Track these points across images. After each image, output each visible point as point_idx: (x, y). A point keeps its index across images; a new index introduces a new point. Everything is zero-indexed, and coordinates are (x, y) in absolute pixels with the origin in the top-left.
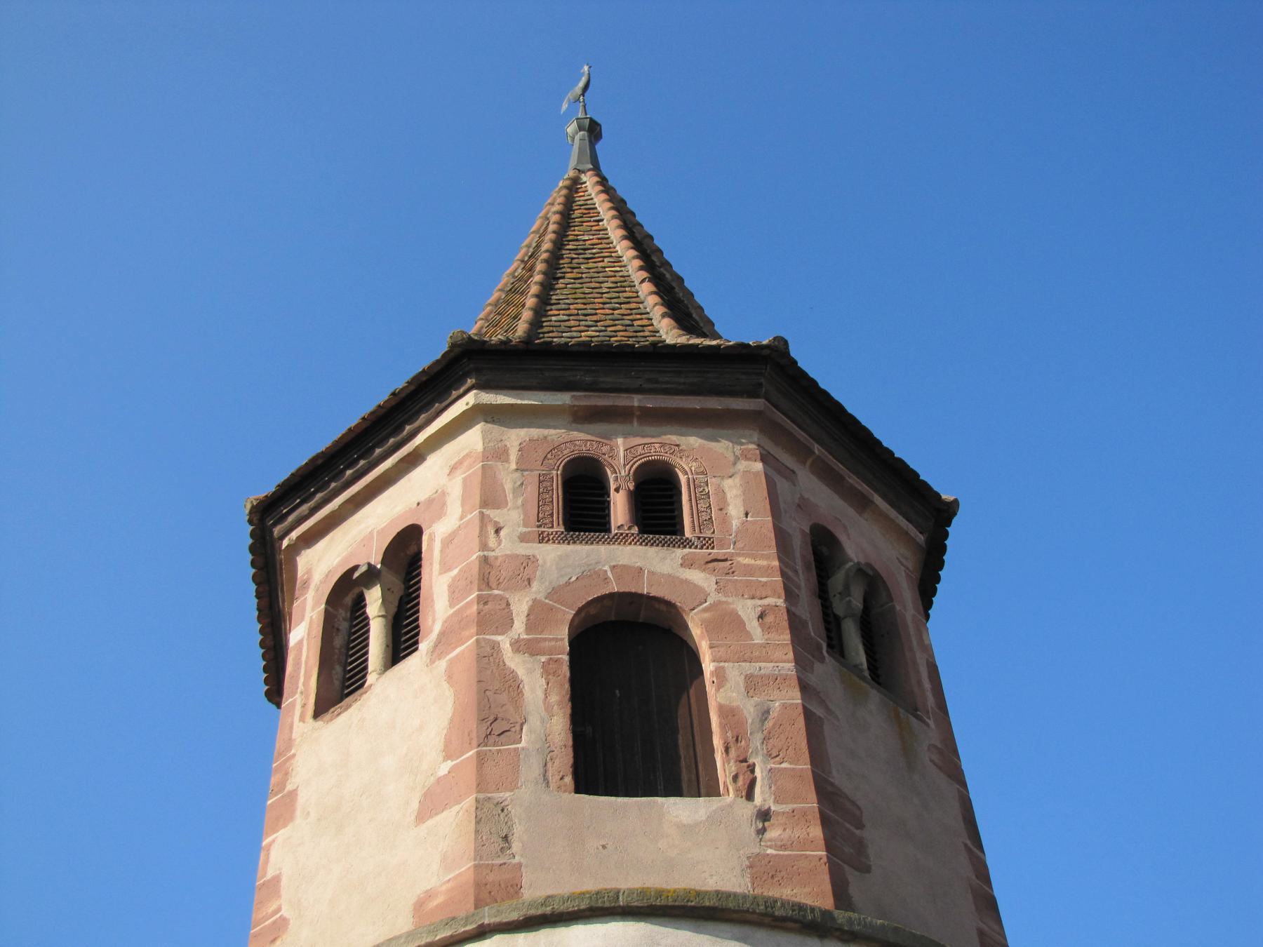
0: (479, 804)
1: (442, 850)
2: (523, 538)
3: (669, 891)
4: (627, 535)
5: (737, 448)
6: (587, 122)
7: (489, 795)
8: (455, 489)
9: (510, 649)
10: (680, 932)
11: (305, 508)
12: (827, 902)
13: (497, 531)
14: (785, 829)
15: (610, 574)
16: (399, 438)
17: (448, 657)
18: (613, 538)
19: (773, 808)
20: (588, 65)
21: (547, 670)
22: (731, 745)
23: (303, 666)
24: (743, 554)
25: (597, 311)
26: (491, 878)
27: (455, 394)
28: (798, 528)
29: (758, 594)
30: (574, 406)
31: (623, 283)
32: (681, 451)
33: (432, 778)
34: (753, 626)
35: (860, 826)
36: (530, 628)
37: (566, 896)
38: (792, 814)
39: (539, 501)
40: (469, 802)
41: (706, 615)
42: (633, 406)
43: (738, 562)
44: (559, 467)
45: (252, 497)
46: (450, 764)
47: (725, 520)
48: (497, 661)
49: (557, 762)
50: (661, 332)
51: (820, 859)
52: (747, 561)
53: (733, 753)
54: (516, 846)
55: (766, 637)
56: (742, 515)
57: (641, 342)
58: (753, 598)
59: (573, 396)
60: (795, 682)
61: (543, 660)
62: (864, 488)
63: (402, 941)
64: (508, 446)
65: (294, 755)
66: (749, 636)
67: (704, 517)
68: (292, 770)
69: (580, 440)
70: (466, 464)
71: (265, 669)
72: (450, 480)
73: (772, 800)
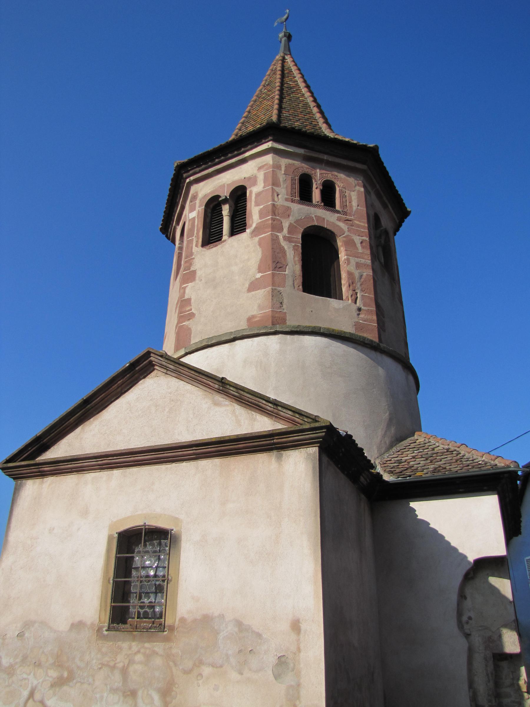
0: (273, 290)
1: (258, 303)
2: (287, 200)
3: (336, 330)
4: (320, 205)
5: (356, 181)
6: (288, 34)
7: (276, 288)
8: (261, 176)
9: (282, 239)
10: (337, 343)
11: (197, 169)
12: (376, 340)
13: (278, 195)
14: (365, 315)
15: (314, 218)
16: (239, 152)
17: (259, 237)
18: (315, 206)
19: (362, 308)
20: (288, 10)
21: (295, 248)
22: (351, 285)
23: (196, 227)
24: (357, 220)
25: (299, 115)
26: (277, 315)
27: (263, 141)
28: (372, 213)
29: (361, 235)
30: (305, 155)
31: (306, 105)
32: (338, 178)
33: (254, 278)
34: (359, 245)
35: (384, 317)
36: (289, 232)
37: (304, 326)
38: (368, 311)
39: (291, 187)
40: (269, 288)
41: (345, 239)
42: (324, 159)
43: (355, 222)
44: (298, 175)
45: (178, 161)
46: (260, 275)
47: (351, 207)
48: (278, 242)
49: (297, 281)
50: (322, 128)
51: (375, 326)
52: (357, 222)
53: (351, 288)
54: (284, 306)
55: (363, 250)
56: (357, 206)
57: (308, 129)
58: (359, 236)
59: (305, 151)
60: (371, 267)
61: (293, 245)
62: (387, 201)
63: (248, 331)
64: (281, 164)
65: (194, 258)
66: (357, 249)
67: (345, 204)
68: (193, 263)
69: (305, 167)
70: (265, 167)
71: (163, 221)
72: (259, 172)
73: (362, 305)
